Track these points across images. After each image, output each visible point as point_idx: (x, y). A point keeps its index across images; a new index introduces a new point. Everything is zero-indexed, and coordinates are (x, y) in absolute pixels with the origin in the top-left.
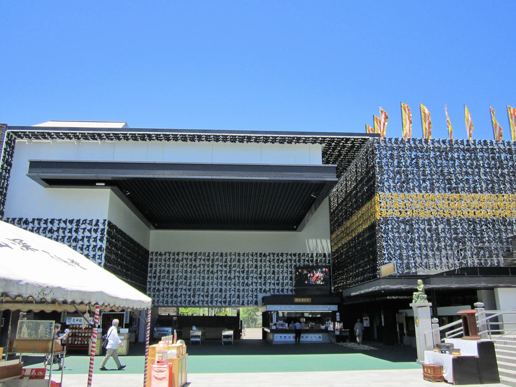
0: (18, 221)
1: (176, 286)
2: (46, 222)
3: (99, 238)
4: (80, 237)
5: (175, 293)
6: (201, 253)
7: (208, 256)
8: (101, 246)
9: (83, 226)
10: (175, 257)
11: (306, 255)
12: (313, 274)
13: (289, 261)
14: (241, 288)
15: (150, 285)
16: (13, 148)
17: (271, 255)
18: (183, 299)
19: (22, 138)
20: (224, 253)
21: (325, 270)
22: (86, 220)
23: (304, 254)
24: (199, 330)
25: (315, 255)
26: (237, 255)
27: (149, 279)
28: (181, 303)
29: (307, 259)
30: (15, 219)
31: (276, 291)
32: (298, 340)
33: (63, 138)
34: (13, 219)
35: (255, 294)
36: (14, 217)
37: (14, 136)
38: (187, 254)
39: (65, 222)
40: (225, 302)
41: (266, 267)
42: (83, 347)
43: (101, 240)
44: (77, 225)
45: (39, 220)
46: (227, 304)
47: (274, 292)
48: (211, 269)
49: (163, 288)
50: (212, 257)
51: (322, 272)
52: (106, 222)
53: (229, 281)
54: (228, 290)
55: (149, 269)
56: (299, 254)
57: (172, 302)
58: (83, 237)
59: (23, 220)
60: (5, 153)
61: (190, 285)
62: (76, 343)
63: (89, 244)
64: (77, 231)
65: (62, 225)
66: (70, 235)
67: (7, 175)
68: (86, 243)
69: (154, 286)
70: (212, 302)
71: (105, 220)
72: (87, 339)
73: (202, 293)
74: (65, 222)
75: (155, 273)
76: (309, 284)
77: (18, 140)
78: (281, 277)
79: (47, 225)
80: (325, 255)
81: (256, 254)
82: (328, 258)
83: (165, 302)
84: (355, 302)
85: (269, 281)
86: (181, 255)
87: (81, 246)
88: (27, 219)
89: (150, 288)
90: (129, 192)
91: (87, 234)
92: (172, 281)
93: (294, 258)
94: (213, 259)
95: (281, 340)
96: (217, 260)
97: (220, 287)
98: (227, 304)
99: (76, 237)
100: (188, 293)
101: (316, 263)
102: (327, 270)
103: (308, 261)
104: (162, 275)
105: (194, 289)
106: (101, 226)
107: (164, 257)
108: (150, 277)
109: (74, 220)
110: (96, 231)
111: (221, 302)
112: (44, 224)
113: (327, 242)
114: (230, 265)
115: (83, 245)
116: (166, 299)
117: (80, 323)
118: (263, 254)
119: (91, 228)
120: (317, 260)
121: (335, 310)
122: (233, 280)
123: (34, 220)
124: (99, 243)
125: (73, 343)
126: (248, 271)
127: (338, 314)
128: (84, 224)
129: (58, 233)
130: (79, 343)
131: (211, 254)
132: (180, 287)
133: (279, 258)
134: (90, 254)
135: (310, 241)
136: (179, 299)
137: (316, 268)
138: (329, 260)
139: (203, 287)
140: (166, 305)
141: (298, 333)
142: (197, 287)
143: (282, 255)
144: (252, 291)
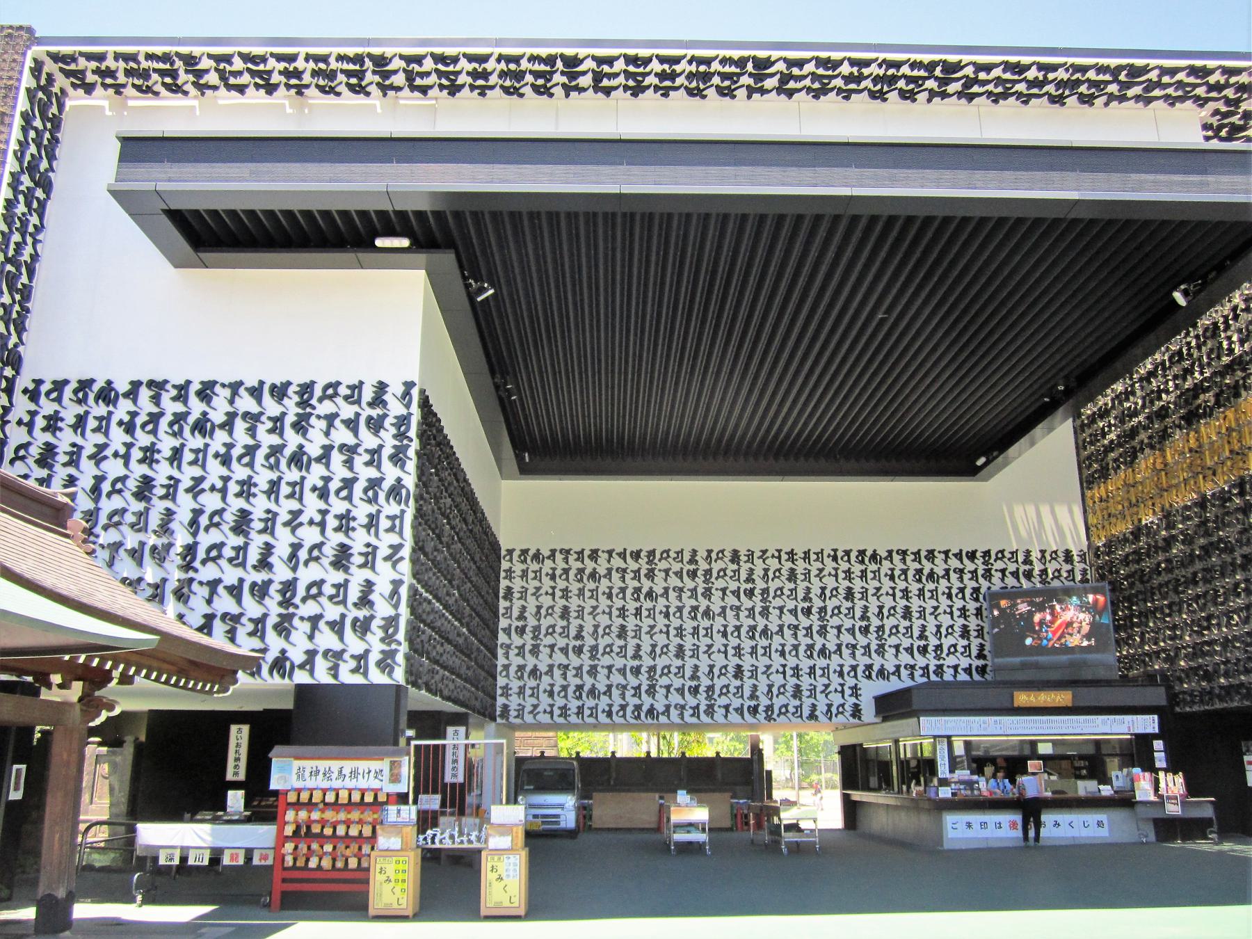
0: (76, 392)
1: (593, 657)
2: (182, 392)
3: (387, 451)
4: (314, 450)
5: (588, 681)
6: (667, 551)
7: (693, 561)
8: (399, 480)
9: (326, 408)
10: (584, 564)
11: (1008, 555)
12: (1053, 614)
13: (954, 576)
14: (805, 664)
15: (507, 656)
16: (56, 123)
17: (896, 558)
18: (618, 701)
19: (89, 89)
20: (743, 552)
21: (1096, 601)
22: (338, 383)
23: (1002, 552)
24: (701, 803)
25: (1035, 555)
26: (784, 557)
27: (502, 638)
28: (609, 714)
29: (1012, 567)
30: (66, 382)
31: (918, 673)
32: (1032, 833)
33: (241, 89)
34: (54, 382)
35: (850, 682)
36: (60, 378)
37: (61, 82)
38: (622, 555)
39: (256, 392)
40: (754, 710)
41: (880, 593)
42: (345, 881)
43: (398, 458)
44: (303, 404)
45: (157, 387)
46: (761, 716)
47: (912, 676)
48: (704, 603)
49: (551, 667)
50: (703, 566)
51: (1084, 607)
52: (415, 392)
53: (765, 642)
54: (761, 669)
55: (503, 604)
56: (987, 553)
57: (580, 711)
58: (328, 449)
59: (96, 387)
60: (25, 130)
61: (636, 656)
62: (313, 863)
63: (349, 475)
64: (301, 426)
65: (246, 403)
66: (275, 440)
67: (34, 219)
68: (339, 471)
69: (520, 661)
70: (710, 711)
71: (409, 385)
72: (354, 847)
73: (677, 683)
74: (256, 392)
75: (521, 617)
76: (1038, 650)
77: (76, 100)
78: (931, 629)
79: (185, 403)
80: (1068, 553)
81: (848, 553)
82: (1079, 567)
83: (557, 712)
84: (1188, 709)
85: (664, 681)
86: (603, 557)
87: (320, 484)
88: (109, 383)
89: (506, 667)
90: (492, 285)
91: (342, 435)
92: (578, 643)
93: (970, 566)
94: (708, 572)
95: (970, 834)
96: (723, 573)
97: (736, 660)
98: (761, 716)
99: (301, 447)
100: (633, 681)
101: (1043, 582)
102: (1101, 598)
103: (1015, 574)
104: (545, 623)
105: (652, 669)
106: (396, 408)
107: (548, 564)
108: (507, 631)
109: (289, 384)
110: (376, 425)
111: (739, 710)
112: (175, 399)
113: (1071, 512)
114: (765, 591)
115: (327, 480)
116: (560, 702)
117: (326, 784)
118: (869, 553)
119: (358, 415)
120: (1044, 572)
121: (1149, 730)
122: (777, 639)
123: (136, 385)
124: (391, 473)
125: (300, 863)
126: (823, 610)
127: (1158, 745)
128: (331, 397)
129: (231, 433)
130: (326, 863)
131: (702, 554)
132: (606, 661)
133: (921, 565)
134: (354, 513)
135: (1018, 511)
136: (605, 700)
137: (1048, 596)
138: (1084, 572)
139: (679, 663)
140: (561, 720)
141: (1031, 810)
142: (661, 662)
143: (931, 555)
144: (841, 674)
